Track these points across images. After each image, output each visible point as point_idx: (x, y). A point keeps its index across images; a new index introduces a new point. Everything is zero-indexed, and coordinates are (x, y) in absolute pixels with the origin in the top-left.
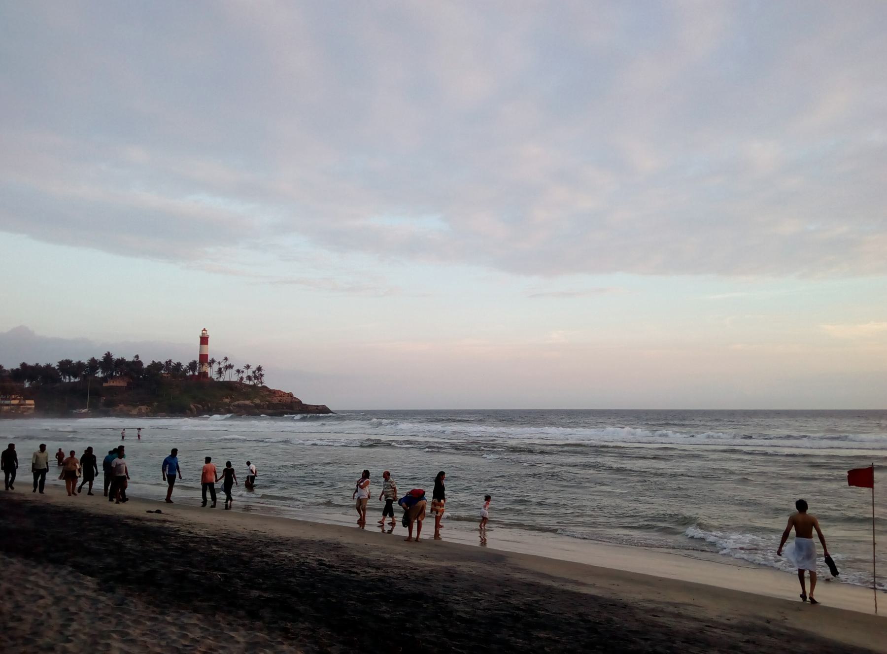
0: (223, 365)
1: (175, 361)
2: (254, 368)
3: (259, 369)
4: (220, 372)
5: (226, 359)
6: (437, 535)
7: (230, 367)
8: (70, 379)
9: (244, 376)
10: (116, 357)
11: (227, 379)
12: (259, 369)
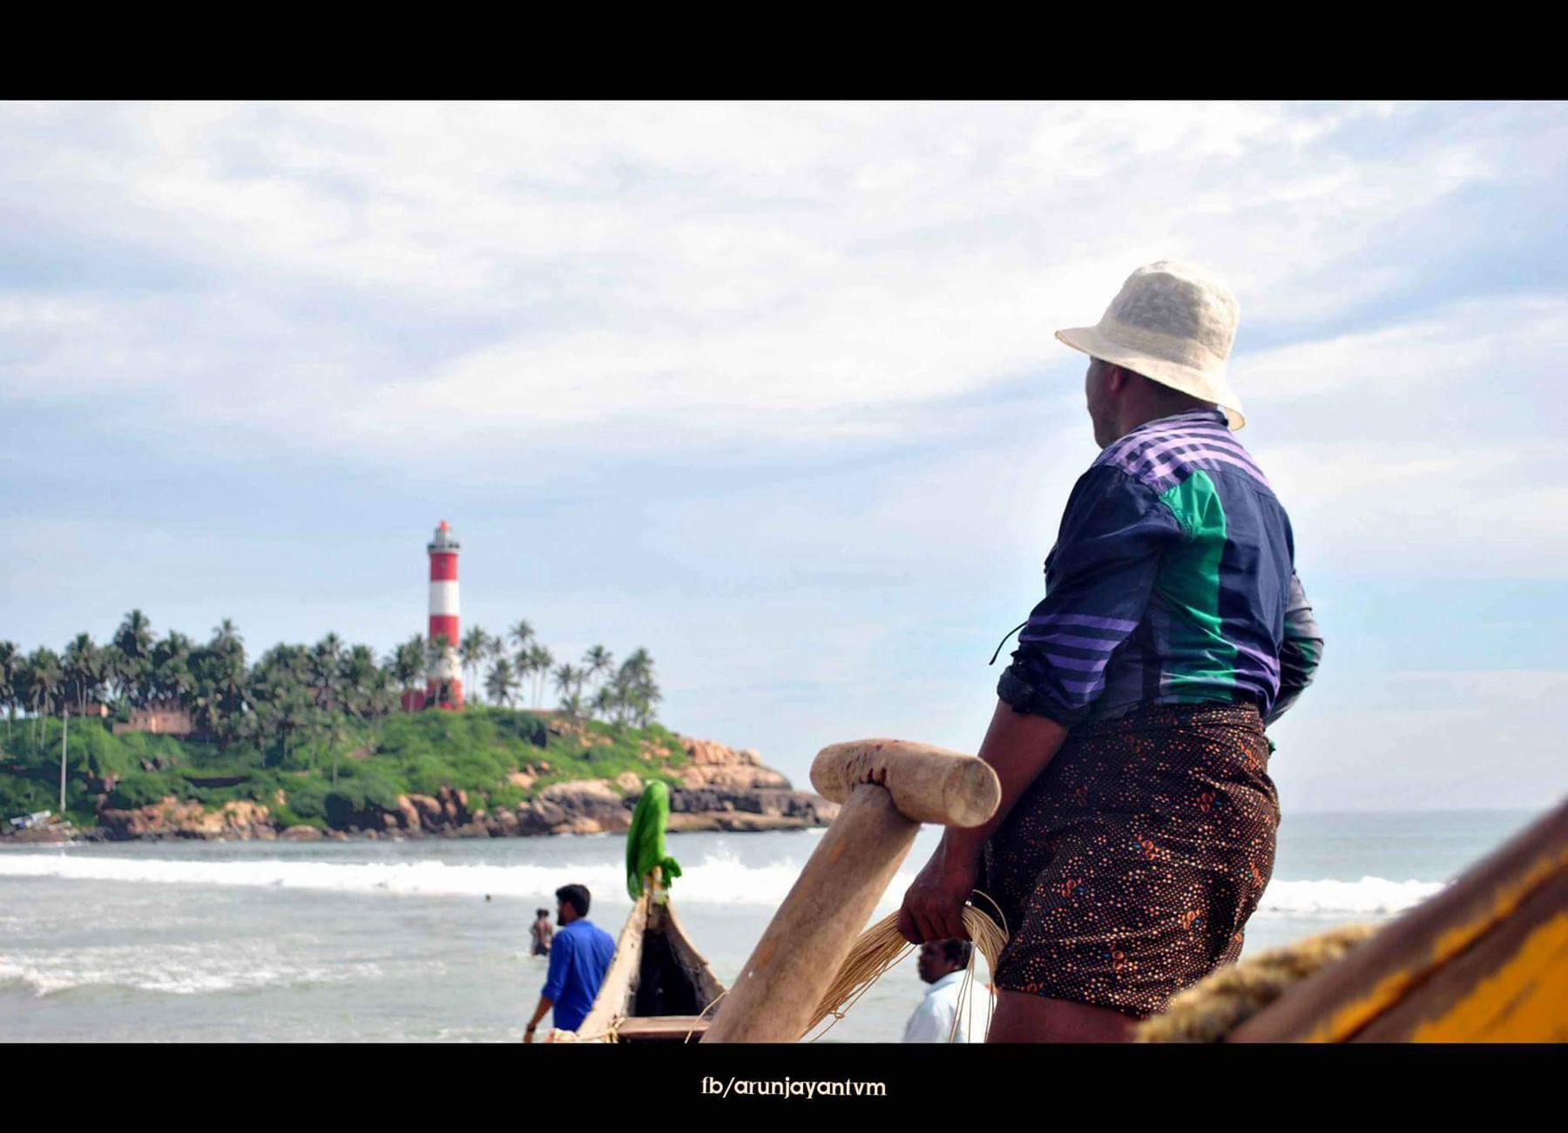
0: (510, 652)
1: (348, 642)
2: (619, 657)
3: (638, 663)
4: (499, 681)
5: (523, 631)
6: (220, 835)
7: (536, 660)
8: (12, 712)
9: (589, 691)
10: (158, 631)
11: (520, 706)
12: (638, 663)
